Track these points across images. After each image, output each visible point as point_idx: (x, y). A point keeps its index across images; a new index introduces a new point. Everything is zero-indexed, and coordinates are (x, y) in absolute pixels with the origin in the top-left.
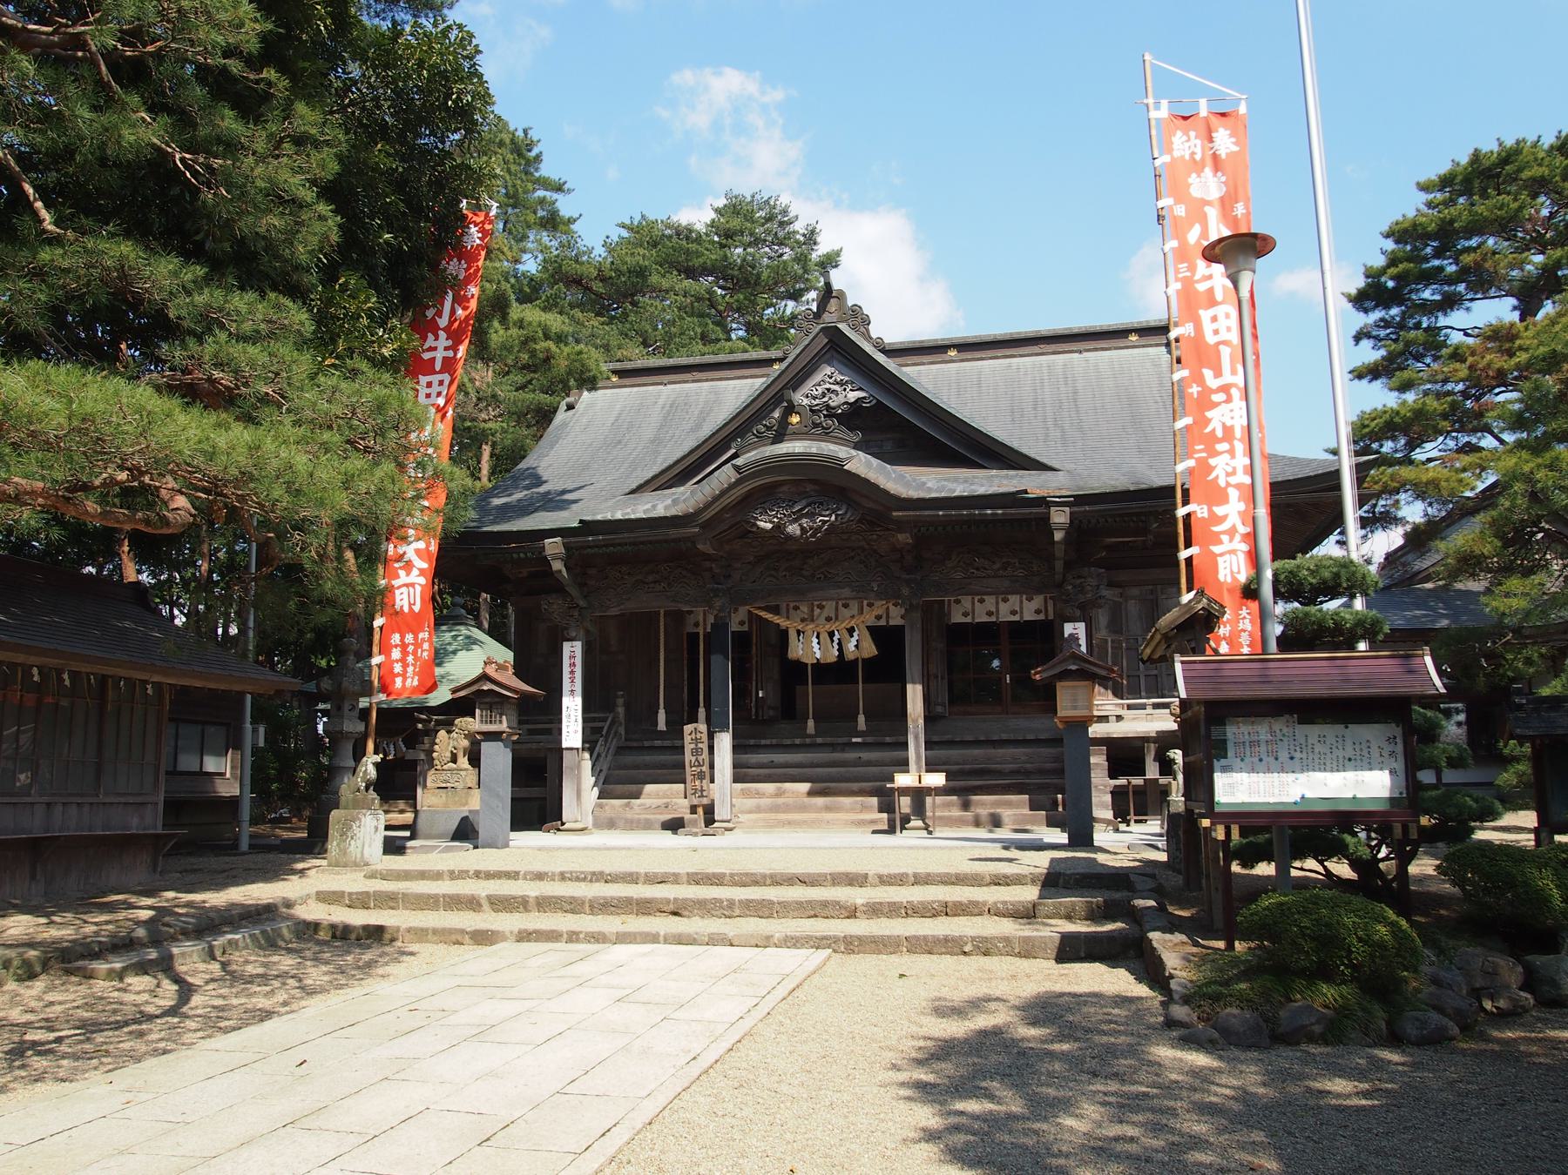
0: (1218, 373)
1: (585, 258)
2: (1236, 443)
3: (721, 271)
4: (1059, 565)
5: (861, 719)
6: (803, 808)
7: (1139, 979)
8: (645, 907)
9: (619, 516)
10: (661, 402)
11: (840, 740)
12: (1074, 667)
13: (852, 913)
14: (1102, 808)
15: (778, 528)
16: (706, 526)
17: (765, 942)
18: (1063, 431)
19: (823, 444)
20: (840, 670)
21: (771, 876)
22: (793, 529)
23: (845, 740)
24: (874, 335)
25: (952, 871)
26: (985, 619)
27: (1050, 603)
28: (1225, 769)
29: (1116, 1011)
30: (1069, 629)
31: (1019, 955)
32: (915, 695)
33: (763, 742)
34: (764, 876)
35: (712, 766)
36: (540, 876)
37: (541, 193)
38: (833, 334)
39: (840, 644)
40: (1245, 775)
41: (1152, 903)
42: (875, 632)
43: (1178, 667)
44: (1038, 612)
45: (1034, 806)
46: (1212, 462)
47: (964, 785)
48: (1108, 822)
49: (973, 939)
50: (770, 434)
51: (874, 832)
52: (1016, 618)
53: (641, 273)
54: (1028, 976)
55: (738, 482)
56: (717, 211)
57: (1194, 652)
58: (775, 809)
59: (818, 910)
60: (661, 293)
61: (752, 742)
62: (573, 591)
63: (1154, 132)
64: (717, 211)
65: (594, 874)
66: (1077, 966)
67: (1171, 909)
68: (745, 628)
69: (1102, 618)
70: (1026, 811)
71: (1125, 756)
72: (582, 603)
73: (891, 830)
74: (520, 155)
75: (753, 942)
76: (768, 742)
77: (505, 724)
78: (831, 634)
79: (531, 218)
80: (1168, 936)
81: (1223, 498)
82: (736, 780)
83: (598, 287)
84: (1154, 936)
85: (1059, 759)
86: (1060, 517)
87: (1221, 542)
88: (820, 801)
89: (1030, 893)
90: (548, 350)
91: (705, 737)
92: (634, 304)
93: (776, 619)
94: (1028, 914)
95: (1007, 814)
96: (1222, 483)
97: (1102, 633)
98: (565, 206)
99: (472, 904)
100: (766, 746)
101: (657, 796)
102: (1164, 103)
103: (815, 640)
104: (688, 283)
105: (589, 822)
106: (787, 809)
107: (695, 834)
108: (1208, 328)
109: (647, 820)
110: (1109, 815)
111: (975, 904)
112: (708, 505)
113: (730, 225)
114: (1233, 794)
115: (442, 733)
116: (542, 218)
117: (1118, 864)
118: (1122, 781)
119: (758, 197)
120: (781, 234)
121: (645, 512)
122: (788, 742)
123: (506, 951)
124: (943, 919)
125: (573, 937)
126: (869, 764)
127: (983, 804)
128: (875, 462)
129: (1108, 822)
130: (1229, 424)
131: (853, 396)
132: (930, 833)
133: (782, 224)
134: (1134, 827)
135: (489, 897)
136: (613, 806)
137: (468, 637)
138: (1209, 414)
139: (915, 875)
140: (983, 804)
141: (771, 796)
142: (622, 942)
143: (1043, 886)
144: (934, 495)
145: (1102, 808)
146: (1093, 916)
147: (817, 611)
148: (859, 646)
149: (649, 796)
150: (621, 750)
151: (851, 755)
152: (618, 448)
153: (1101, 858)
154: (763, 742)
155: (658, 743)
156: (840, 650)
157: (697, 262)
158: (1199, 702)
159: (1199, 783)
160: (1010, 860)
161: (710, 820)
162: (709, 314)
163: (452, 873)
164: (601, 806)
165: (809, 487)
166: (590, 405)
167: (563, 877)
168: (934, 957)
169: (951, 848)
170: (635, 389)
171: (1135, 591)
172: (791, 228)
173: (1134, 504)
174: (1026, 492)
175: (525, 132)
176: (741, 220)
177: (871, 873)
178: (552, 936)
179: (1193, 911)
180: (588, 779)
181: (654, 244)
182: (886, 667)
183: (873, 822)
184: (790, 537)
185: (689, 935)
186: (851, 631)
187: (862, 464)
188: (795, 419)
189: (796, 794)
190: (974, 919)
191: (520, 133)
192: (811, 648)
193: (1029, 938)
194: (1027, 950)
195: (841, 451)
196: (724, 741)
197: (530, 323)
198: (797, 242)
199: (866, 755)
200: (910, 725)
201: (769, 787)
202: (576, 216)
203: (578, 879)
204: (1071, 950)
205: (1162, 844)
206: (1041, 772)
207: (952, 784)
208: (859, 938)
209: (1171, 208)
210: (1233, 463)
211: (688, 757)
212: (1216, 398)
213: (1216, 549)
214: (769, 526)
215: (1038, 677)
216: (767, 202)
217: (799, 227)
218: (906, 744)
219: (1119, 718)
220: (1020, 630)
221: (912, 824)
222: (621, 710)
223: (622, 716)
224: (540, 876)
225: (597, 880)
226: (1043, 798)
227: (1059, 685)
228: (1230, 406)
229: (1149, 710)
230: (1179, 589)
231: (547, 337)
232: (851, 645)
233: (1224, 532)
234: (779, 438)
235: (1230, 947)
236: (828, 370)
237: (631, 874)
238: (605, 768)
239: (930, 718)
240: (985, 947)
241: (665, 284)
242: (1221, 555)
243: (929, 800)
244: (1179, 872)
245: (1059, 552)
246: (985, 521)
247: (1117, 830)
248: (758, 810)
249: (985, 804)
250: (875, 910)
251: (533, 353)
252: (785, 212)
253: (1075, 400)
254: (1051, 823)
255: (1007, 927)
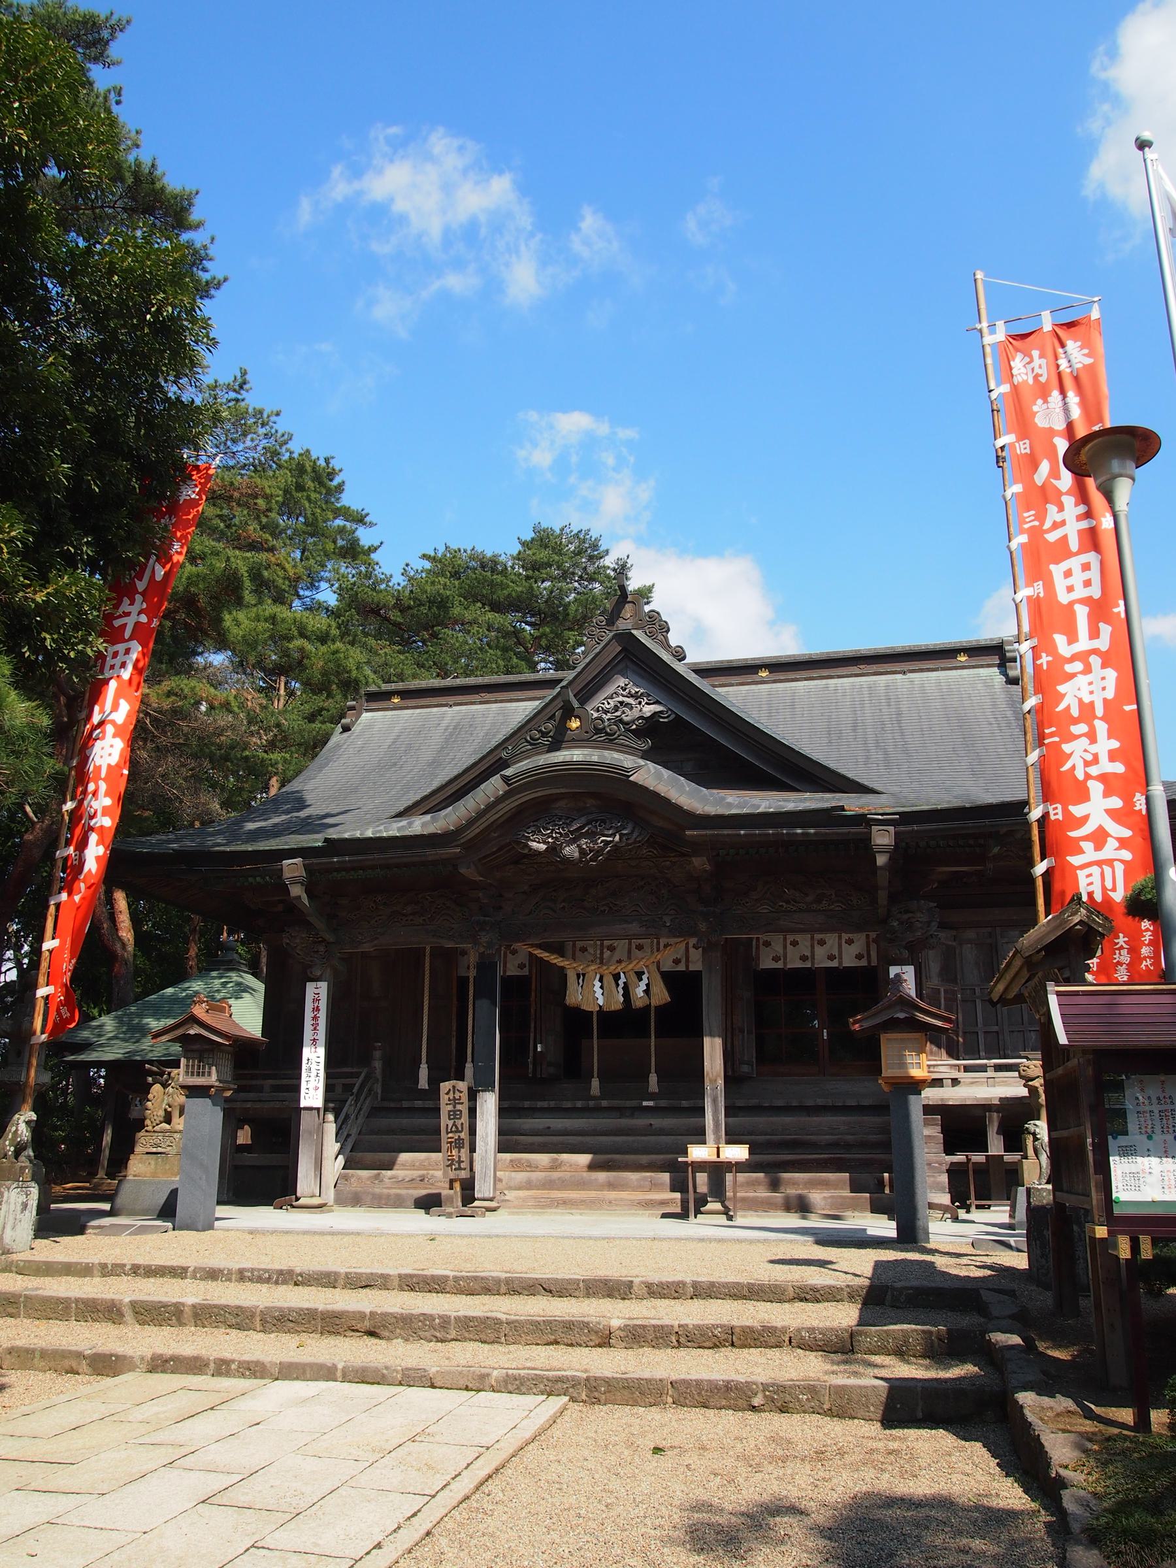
0: (1072, 639)
1: (383, 586)
2: (1097, 723)
3: (522, 604)
4: (882, 896)
5: (653, 1078)
6: (581, 1185)
7: (1007, 1468)
8: (332, 1324)
9: (369, 834)
10: (444, 723)
11: (629, 1104)
12: (901, 1015)
13: (605, 1339)
14: (933, 1189)
15: (553, 850)
16: (469, 846)
17: (477, 1383)
18: (886, 753)
19: (606, 753)
20: (626, 1021)
21: (508, 1281)
22: (571, 851)
23: (634, 1103)
24: (673, 643)
25: (743, 1279)
26: (799, 964)
27: (873, 947)
28: (1128, 1151)
29: (977, 1544)
30: (893, 971)
31: (830, 1413)
32: (713, 1052)
33: (540, 1104)
34: (498, 1281)
35: (473, 1132)
36: (213, 1275)
37: (339, 522)
38: (627, 641)
39: (626, 987)
40: (1154, 1161)
41: (1016, 1340)
42: (669, 979)
43: (1053, 1000)
44: (859, 957)
45: (855, 1187)
46: (1067, 748)
47: (772, 1159)
48: (944, 1209)
49: (765, 1387)
50: (546, 741)
51: (664, 1216)
52: (835, 964)
53: (441, 604)
54: (841, 1453)
55: (507, 795)
56: (523, 544)
57: (1067, 981)
58: (549, 1185)
59: (559, 1335)
60: (465, 625)
61: (527, 1104)
62: (318, 923)
63: (989, 361)
64: (523, 544)
65: (280, 1273)
66: (912, 1433)
67: (1041, 1346)
68: (526, 972)
69: (934, 967)
70: (846, 1193)
71: (962, 1127)
72: (330, 937)
73: (683, 1215)
74: (321, 484)
75: (462, 1383)
76: (545, 1104)
77: (214, 1077)
78: (617, 977)
79: (330, 546)
80: (1046, 1401)
81: (1083, 795)
82: (502, 1148)
83: (395, 616)
84: (1026, 1398)
85: (885, 1130)
86: (883, 838)
87: (1081, 851)
88: (602, 1176)
89: (845, 1316)
90: (302, 650)
91: (465, 1097)
92: (434, 635)
93: (555, 960)
94: (842, 1347)
95: (817, 1197)
96: (1080, 775)
97: (934, 982)
98: (366, 537)
99: (109, 1312)
100: (542, 1109)
101: (413, 1167)
102: (1000, 324)
103: (598, 984)
104: (490, 615)
105: (330, 1195)
106: (563, 1185)
107: (449, 1215)
108: (1060, 584)
109: (398, 1196)
110: (945, 1199)
111: (770, 1330)
112: (471, 822)
113: (537, 557)
114: (1138, 1188)
115: (157, 1088)
116: (342, 547)
117: (963, 1273)
118: (960, 1158)
119: (567, 530)
120: (591, 569)
121: (399, 829)
122: (569, 1105)
123: (130, 1383)
124: (727, 1351)
125: (223, 1368)
126: (662, 1132)
127: (795, 1183)
128: (666, 773)
129: (944, 1209)
130: (1086, 700)
131: (648, 710)
132: (730, 1218)
133: (591, 558)
134: (976, 1215)
135: (133, 1304)
136: (359, 1178)
137: (239, 984)
138: (1061, 688)
139: (695, 1285)
140: (795, 1183)
141: (545, 1170)
142: (285, 1378)
143: (864, 1304)
144: (734, 811)
145: (933, 1189)
146: (937, 1352)
147: (607, 954)
148: (647, 991)
149: (404, 1166)
150: (375, 1111)
151: (640, 1122)
152: (387, 767)
153: (940, 1262)
154: (540, 1104)
155: (419, 1104)
156: (627, 994)
157: (501, 594)
158: (1085, 1051)
159: (1082, 1167)
160: (822, 1264)
161: (468, 1196)
162: (513, 647)
163: (104, 1266)
164: (346, 1178)
165: (590, 802)
166: (370, 725)
167: (242, 1276)
168: (711, 1413)
169: (751, 1242)
170: (418, 711)
171: (971, 934)
172: (602, 562)
173: (970, 823)
174: (842, 808)
175: (327, 460)
176: (550, 552)
177: (636, 1280)
178: (193, 1365)
179: (1074, 1351)
180: (331, 1146)
181: (456, 575)
182: (681, 1017)
183: (663, 1203)
184: (567, 861)
185: (377, 1370)
186: (639, 975)
187: (651, 775)
188: (574, 724)
189: (574, 1167)
190: (770, 1353)
191: (322, 463)
192: (595, 994)
193: (843, 1387)
194: (841, 1406)
195: (627, 761)
196: (489, 1104)
197: (283, 620)
198: (608, 577)
199: (657, 1122)
200: (708, 1087)
201: (543, 1159)
202: (376, 544)
203: (260, 1280)
204: (905, 1408)
205: (1018, 1238)
206: (863, 1145)
207: (758, 1158)
208: (607, 1381)
209: (1012, 445)
210: (1093, 748)
211: (445, 1121)
212: (1069, 668)
213: (1075, 860)
214: (543, 847)
215: (857, 1027)
216: (577, 535)
217: (609, 561)
218: (702, 1110)
219: (955, 1082)
220: (839, 978)
221: (710, 1206)
222: (378, 1064)
223: (378, 1073)
224: (213, 1275)
225: (285, 1282)
226: (866, 1177)
227: (884, 1038)
228: (1089, 678)
229: (991, 1073)
230: (1036, 912)
231: (302, 635)
232: (639, 990)
233: (1086, 838)
234: (555, 746)
235: (1143, 1423)
236: (622, 682)
237: (328, 1275)
238: (354, 1132)
239: (732, 1079)
240: (781, 1399)
241: (468, 616)
242: (1083, 867)
243: (729, 1177)
244: (1047, 1287)
245: (883, 879)
246: (790, 843)
247: (956, 1219)
248: (528, 1186)
249: (796, 1181)
250: (636, 1336)
251: (286, 653)
252: (595, 546)
253: (899, 722)
254: (876, 1208)
255: (811, 1367)
